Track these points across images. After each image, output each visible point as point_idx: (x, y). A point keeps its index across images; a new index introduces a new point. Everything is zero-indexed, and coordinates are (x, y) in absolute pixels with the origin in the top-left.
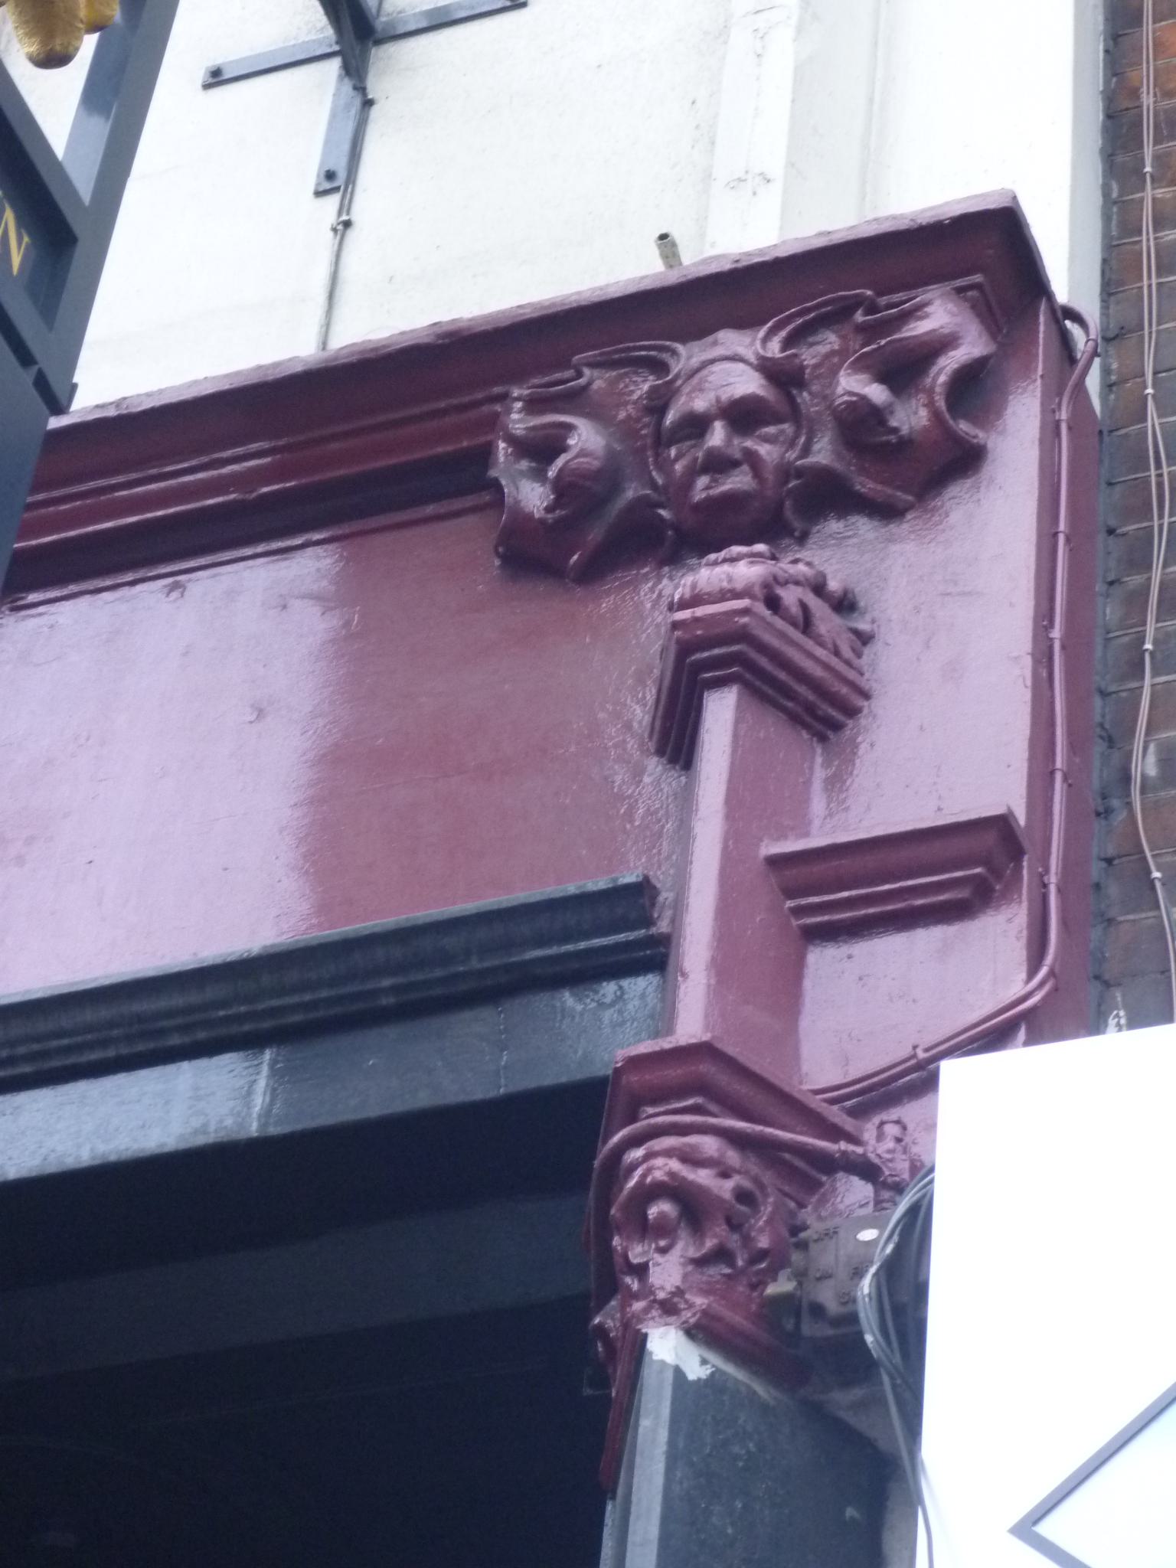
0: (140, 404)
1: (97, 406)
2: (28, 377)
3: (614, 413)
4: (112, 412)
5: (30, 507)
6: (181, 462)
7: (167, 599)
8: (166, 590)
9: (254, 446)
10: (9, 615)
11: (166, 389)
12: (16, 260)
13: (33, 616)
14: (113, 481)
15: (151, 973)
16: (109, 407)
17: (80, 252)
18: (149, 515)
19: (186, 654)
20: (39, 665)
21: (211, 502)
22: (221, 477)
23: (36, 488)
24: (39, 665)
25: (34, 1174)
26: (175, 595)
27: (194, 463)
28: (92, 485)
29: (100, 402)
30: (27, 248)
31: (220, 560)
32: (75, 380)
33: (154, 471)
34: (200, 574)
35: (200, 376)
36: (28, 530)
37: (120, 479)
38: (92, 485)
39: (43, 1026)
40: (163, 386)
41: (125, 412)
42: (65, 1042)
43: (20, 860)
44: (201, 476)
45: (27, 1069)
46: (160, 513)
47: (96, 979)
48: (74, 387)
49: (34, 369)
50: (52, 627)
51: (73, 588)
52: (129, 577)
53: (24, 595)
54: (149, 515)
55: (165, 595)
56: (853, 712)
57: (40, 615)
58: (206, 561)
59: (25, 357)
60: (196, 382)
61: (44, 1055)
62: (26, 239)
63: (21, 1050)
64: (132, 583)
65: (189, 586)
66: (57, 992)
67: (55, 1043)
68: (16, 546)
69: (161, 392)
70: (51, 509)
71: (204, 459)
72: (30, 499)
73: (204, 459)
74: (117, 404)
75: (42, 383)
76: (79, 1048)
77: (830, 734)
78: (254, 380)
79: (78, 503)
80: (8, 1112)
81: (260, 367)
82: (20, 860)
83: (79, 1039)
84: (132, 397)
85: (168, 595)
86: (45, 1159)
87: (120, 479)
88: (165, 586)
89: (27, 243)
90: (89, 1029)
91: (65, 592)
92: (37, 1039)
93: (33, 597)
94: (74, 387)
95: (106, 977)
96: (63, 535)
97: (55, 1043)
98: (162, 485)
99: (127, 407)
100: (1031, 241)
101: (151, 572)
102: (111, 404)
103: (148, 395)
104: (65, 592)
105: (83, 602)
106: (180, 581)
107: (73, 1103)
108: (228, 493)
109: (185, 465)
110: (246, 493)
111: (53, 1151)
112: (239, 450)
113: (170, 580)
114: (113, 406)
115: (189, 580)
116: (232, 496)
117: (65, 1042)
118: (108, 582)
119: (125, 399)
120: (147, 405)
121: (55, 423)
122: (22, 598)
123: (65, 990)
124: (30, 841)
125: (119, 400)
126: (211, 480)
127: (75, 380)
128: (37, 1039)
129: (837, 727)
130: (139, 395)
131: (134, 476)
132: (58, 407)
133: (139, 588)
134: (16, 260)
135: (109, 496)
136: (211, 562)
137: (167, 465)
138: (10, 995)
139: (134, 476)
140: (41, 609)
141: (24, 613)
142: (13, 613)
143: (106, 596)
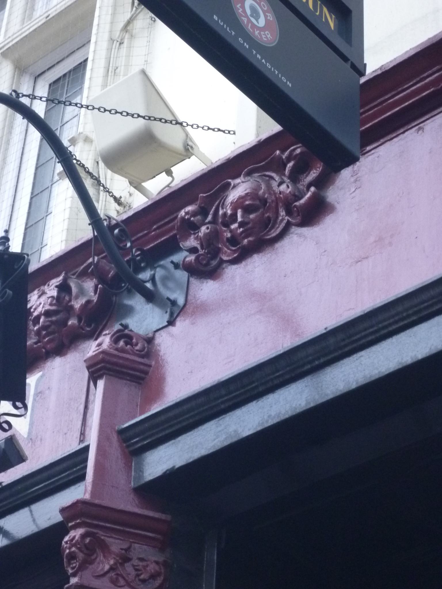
0: (388, 67)
1: (373, 72)
2: (348, 66)
3: (124, 239)
4: (379, 72)
5: (362, 114)
6: (409, 82)
7: (418, 134)
8: (417, 131)
9: (435, 69)
10: (362, 157)
11: (397, 57)
12: (332, 25)
13: (369, 155)
14: (386, 97)
15: (209, 386)
16: (378, 70)
17: (354, 14)
18: (403, 106)
19: (430, 153)
20: (378, 172)
21: (424, 94)
22: (426, 84)
23: (362, 106)
24: (378, 172)
25: (428, 355)
26: (420, 132)
27: (414, 81)
28: (379, 101)
29: (374, 70)
30: (334, 21)
31: (434, 114)
32: (365, 62)
33: (400, 89)
34: (428, 122)
35: (408, 49)
36: (364, 122)
37: (389, 95)
38: (379, 101)
39: (416, 301)
40: (395, 57)
41: (384, 70)
42: (426, 304)
43: (390, 244)
44: (418, 85)
45: (414, 318)
46: (407, 104)
47: (431, 279)
48: (365, 65)
49: (350, 62)
50: (378, 157)
51: (382, 141)
52: (402, 130)
53: (365, 148)
54: (403, 106)
55: (417, 133)
56: (146, 373)
57: (373, 154)
58: (429, 116)
59: (345, 59)
60: (407, 52)
61: (420, 311)
62: (333, 16)
63: (410, 312)
64: (404, 132)
65: (425, 127)
66: (418, 287)
67: (422, 306)
68: (361, 129)
69: (395, 59)
70: (367, 114)
71: (418, 79)
72: (362, 111)
73: (418, 79)
74: (380, 68)
75: (354, 67)
76: (390, 325)
77: (141, 382)
78: (428, 44)
79: (376, 109)
80: (412, 335)
81: (429, 39)
82: (390, 244)
83: (430, 302)
84: (385, 64)
85: (418, 133)
86: (430, 349)
87: (389, 95)
88: (416, 130)
89: (334, 18)
90: (433, 298)
91: (379, 143)
92: (416, 306)
93: (368, 148)
94: (365, 65)
95: (435, 277)
96: (373, 122)
97: (422, 306)
98: (405, 93)
99: (384, 68)
100: (434, 41)
101: (409, 126)
102: (378, 69)
103: (391, 62)
104: (379, 143)
105: (388, 144)
106: (421, 127)
107: (435, 326)
108: (430, 89)
109: (411, 83)
110: (437, 86)
111: (432, 345)
112: (430, 72)
113: (417, 127)
114: (379, 69)
115: (424, 125)
116: (432, 90)
117: (426, 304)
118: (394, 135)
119: (383, 66)
120: (391, 65)
121: (363, 80)
122: (364, 150)
123: (421, 286)
124: (392, 236)
125: (381, 67)
126: (405, 96)
127: (365, 62)
128: (416, 306)
129: (143, 379)
130: (387, 63)
131: (393, 93)
132: (362, 74)
133: (406, 133)
134: (332, 25)
135: (387, 103)
136: (431, 116)
137: (404, 85)
138: (401, 293)
139: (393, 93)
140: (373, 152)
141: (366, 155)
142: (363, 156)
143: (395, 140)
